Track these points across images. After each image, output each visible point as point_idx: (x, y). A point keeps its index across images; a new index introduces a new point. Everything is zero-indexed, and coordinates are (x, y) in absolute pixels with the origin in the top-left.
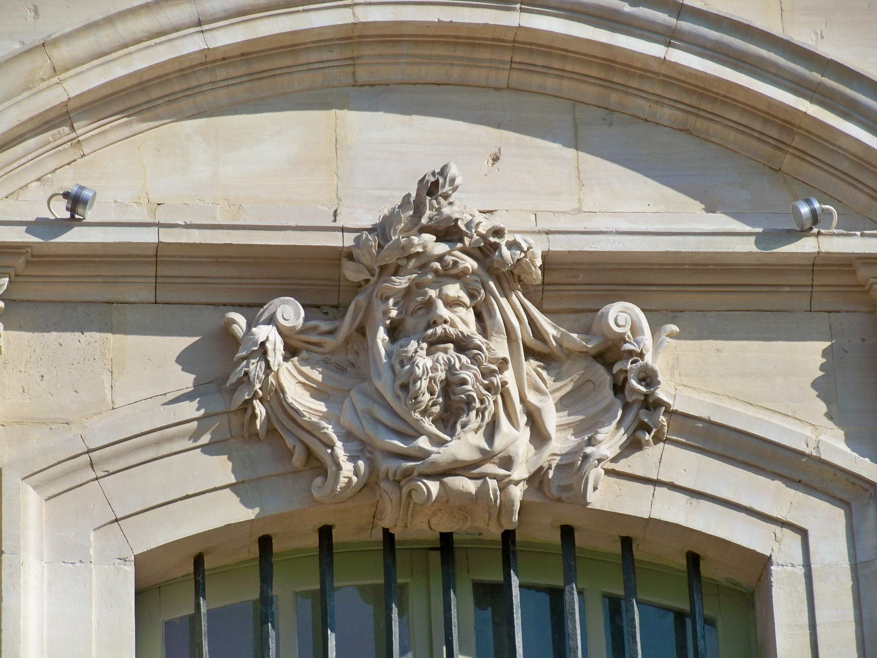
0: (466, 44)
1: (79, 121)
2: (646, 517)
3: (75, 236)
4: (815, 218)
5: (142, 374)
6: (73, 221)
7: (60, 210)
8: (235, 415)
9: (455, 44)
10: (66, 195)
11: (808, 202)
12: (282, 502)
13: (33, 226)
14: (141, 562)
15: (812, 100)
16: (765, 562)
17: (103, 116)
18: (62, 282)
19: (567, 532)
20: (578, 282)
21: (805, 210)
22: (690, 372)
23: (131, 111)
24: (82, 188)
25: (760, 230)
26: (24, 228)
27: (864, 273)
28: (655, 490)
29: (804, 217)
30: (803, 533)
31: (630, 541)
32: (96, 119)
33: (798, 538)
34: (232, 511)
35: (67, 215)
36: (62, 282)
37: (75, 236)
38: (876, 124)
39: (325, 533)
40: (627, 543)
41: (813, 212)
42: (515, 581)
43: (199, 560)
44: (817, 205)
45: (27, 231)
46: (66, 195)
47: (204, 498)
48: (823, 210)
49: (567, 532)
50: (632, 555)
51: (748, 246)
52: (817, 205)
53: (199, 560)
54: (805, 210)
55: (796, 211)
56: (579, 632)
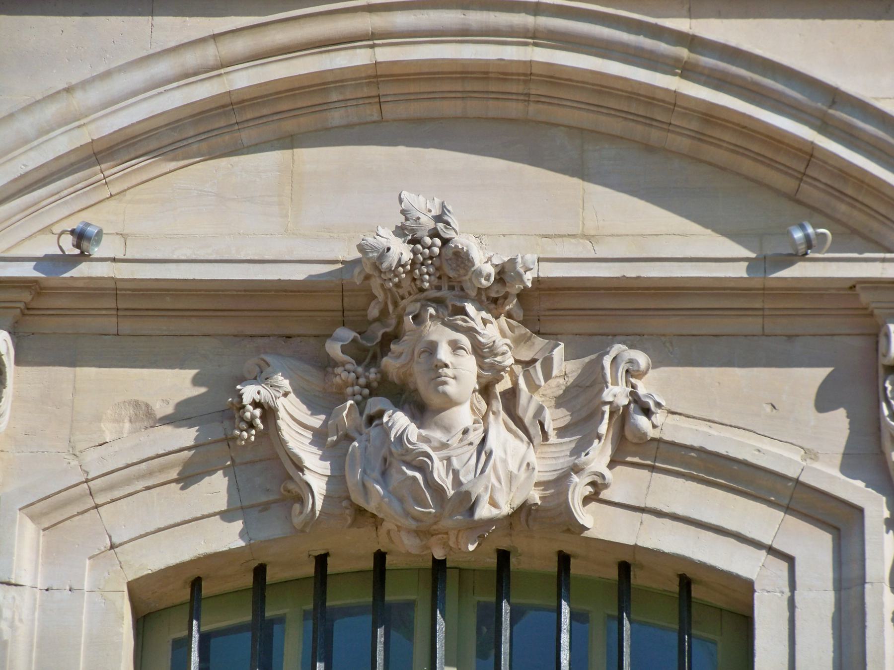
0: (498, 79)
1: (106, 162)
2: (632, 544)
3: (83, 270)
4: (809, 243)
5: (130, 406)
6: (84, 256)
7: (68, 245)
8: (233, 443)
9: (463, 79)
10: (73, 232)
11: (802, 227)
12: (273, 529)
13: (42, 262)
14: (136, 590)
15: (609, 26)
16: (748, 586)
17: (127, 158)
18: (62, 316)
19: (564, 560)
20: (544, 306)
21: (798, 235)
22: (689, 401)
23: (155, 154)
24: (88, 225)
25: (753, 255)
26: (34, 263)
27: (865, 298)
28: (634, 514)
29: (798, 242)
30: (790, 560)
31: (627, 565)
32: (119, 161)
33: (784, 566)
34: (229, 537)
35: (77, 252)
36: (62, 316)
37: (83, 270)
38: (893, 159)
39: (321, 561)
40: (625, 568)
41: (807, 237)
42: (506, 607)
43: (196, 584)
44: (810, 230)
45: (35, 268)
46: (73, 232)
47: (203, 526)
48: (818, 235)
49: (564, 560)
50: (629, 581)
51: (739, 271)
52: (810, 230)
53: (196, 584)
54: (798, 235)
55: (789, 234)
56: (626, 650)
